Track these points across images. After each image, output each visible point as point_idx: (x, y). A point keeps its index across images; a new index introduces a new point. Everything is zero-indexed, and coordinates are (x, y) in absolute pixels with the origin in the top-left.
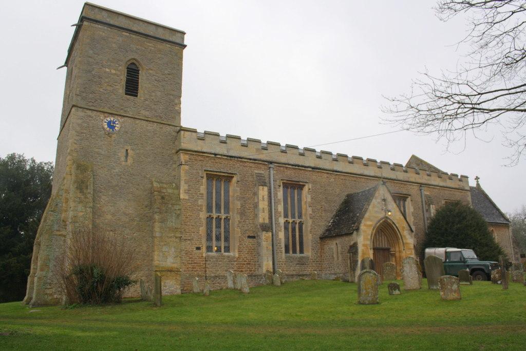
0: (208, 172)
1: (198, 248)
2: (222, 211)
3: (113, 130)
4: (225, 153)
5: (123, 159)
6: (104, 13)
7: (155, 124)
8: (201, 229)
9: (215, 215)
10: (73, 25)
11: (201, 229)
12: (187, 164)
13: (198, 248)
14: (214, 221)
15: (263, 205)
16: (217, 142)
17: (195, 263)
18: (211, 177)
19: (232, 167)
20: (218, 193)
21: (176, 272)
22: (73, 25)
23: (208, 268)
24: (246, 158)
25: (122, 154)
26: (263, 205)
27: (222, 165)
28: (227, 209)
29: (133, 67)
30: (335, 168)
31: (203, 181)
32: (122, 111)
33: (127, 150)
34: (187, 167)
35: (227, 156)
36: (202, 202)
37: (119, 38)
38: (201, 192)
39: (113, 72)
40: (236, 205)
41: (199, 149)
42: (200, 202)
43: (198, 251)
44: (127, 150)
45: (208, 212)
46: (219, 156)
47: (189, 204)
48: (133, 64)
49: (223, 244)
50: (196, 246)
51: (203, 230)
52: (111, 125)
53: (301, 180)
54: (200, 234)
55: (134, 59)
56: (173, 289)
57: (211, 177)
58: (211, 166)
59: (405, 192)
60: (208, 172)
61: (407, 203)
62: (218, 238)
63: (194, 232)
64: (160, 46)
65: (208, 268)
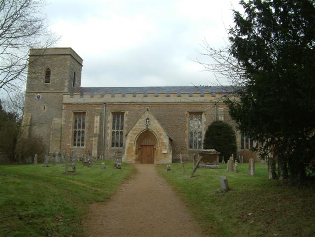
5: (43, 110)
14: (116, 133)
15: (97, 124)
18: (75, 113)
19: (119, 106)
20: (118, 121)
25: (42, 108)
26: (97, 124)
28: (122, 129)
29: (49, 70)
30: (145, 101)
36: (71, 125)
40: (87, 125)
45: (113, 129)
49: (80, 143)
53: (122, 110)
57: (75, 113)
58: (193, 108)
59: (202, 109)
61: (203, 116)
62: (79, 140)
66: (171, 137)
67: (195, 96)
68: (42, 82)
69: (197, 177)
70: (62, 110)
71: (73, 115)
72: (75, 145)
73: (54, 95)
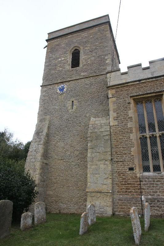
0: (134, 98)
1: (131, 169)
2: (157, 129)
3: (63, 92)
4: (150, 76)
5: (69, 108)
6: (104, 18)
7: (91, 78)
8: (132, 149)
9: (148, 134)
10: (44, 48)
11: (132, 149)
12: (114, 96)
13: (131, 169)
14: (148, 140)
16: (141, 70)
17: (128, 184)
18: (138, 100)
21: (106, 194)
22: (44, 48)
23: (144, 189)
24: (143, 80)
27: (148, 87)
31: (131, 106)
32: (69, 79)
33: (73, 102)
34: (114, 99)
35: (152, 78)
37: (64, 41)
38: (130, 116)
39: (63, 59)
41: (124, 81)
42: (129, 125)
43: (132, 172)
44: (73, 102)
46: (143, 81)
47: (120, 129)
48: (76, 49)
50: (129, 166)
51: (135, 150)
52: (62, 90)
54: (132, 154)
55: (75, 47)
56: (103, 210)
57: (138, 100)
60: (134, 98)
63: (126, 154)
64: (92, 31)
65: (144, 189)
66: (32, 144)
67: (109, 215)
68: (68, 67)
69: (84, 77)
70: (108, 98)
71: (132, 104)
72: (146, 169)
73: (87, 81)
